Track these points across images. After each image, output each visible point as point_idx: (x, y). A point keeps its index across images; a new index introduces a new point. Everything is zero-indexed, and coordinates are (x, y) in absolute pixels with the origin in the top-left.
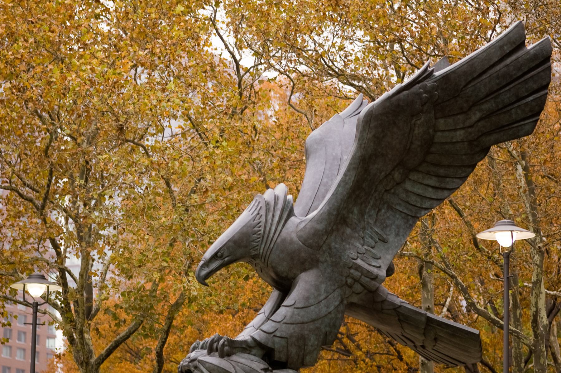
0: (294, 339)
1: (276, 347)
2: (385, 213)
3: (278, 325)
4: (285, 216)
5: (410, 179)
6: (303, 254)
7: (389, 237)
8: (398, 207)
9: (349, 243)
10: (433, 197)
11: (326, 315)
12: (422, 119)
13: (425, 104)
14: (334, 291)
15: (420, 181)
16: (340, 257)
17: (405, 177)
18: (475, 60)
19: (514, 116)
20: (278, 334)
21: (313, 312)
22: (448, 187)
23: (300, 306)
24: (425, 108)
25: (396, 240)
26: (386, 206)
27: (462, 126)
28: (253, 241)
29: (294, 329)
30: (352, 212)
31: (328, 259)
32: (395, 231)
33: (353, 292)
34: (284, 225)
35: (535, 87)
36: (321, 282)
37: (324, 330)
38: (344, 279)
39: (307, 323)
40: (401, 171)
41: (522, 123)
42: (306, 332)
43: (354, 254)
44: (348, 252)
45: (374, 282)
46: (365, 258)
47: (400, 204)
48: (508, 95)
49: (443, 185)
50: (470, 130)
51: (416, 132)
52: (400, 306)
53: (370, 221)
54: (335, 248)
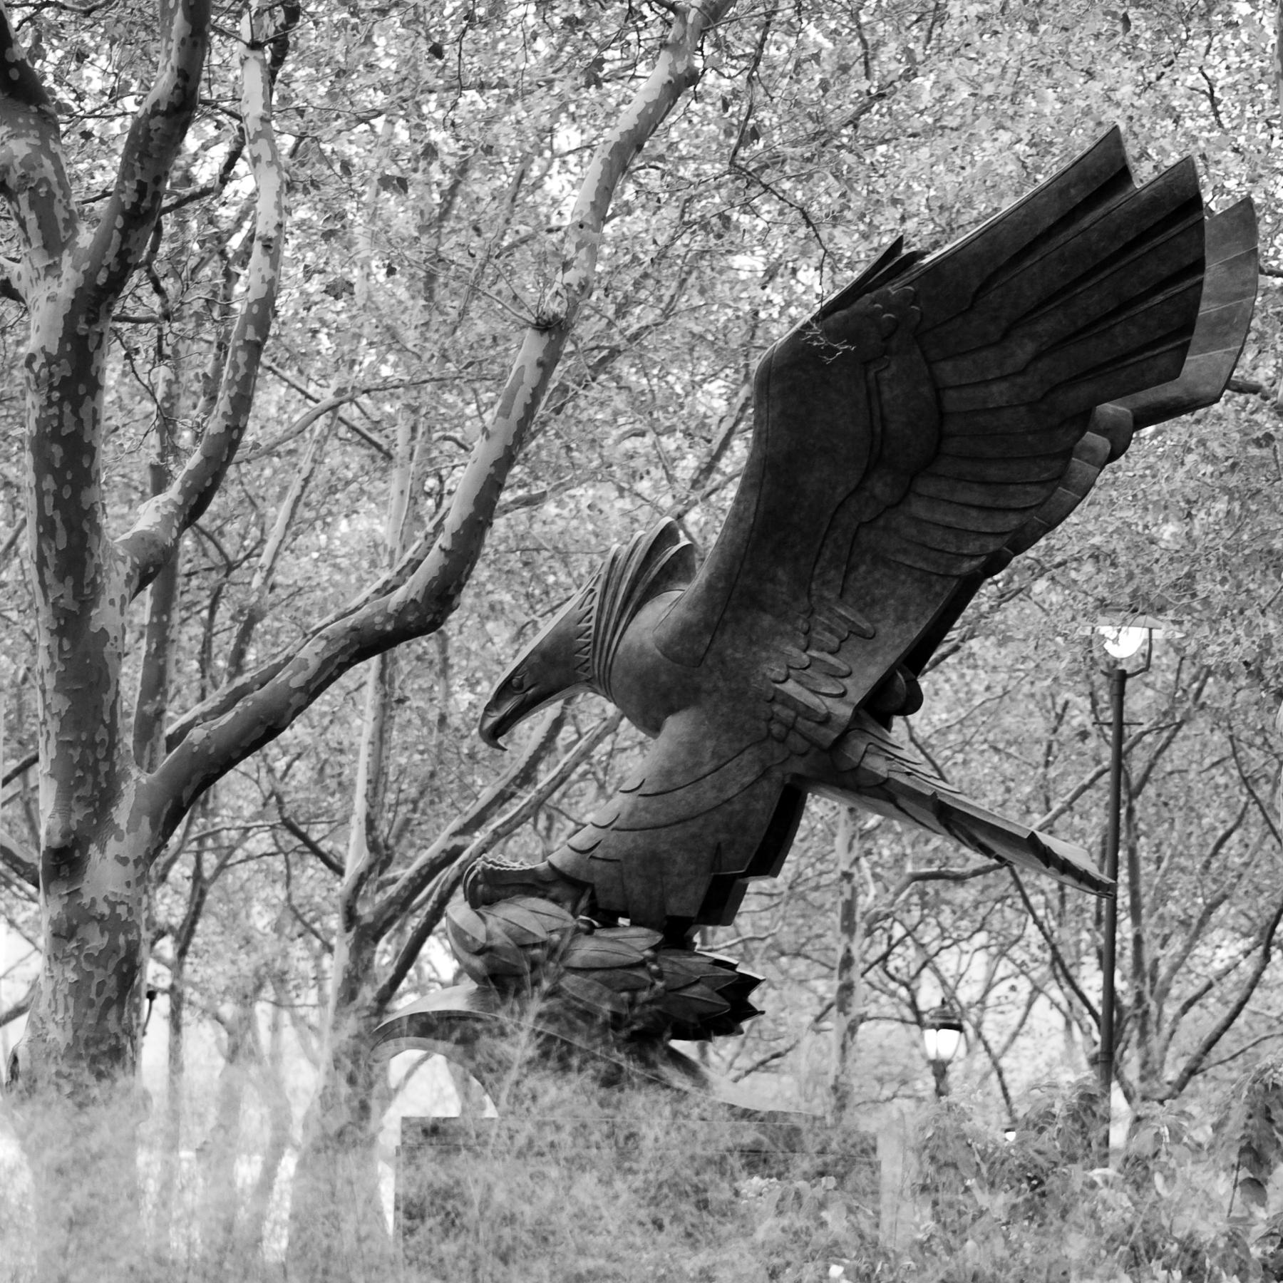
0: (635, 863)
1: (597, 879)
2: (869, 572)
3: (601, 834)
4: (637, 595)
5: (920, 495)
6: (664, 678)
7: (879, 625)
8: (901, 558)
9: (766, 648)
10: (984, 529)
11: (716, 808)
12: (894, 368)
13: (892, 334)
14: (742, 752)
15: (946, 497)
16: (746, 679)
17: (907, 493)
18: (1000, 227)
19: (1121, 341)
20: (599, 852)
21: (683, 800)
22: (1014, 504)
23: (647, 789)
24: (894, 344)
25: (897, 631)
26: (868, 557)
27: (997, 373)
28: (579, 651)
29: (634, 841)
30: (773, 580)
31: (721, 684)
32: (895, 610)
33: (792, 753)
34: (633, 616)
35: (1165, 271)
36: (705, 737)
37: (711, 840)
38: (763, 725)
39: (666, 826)
40: (889, 479)
41: (1148, 354)
42: (664, 847)
43: (777, 671)
44: (764, 667)
45: (823, 730)
46: (804, 679)
47: (905, 552)
48: (1096, 297)
49: (1001, 502)
50: (1020, 380)
51: (887, 395)
52: (888, 780)
53: (826, 594)
54: (734, 660)
